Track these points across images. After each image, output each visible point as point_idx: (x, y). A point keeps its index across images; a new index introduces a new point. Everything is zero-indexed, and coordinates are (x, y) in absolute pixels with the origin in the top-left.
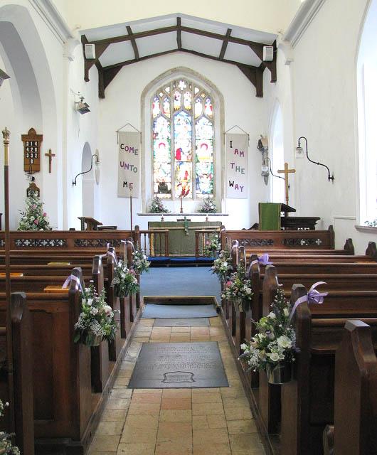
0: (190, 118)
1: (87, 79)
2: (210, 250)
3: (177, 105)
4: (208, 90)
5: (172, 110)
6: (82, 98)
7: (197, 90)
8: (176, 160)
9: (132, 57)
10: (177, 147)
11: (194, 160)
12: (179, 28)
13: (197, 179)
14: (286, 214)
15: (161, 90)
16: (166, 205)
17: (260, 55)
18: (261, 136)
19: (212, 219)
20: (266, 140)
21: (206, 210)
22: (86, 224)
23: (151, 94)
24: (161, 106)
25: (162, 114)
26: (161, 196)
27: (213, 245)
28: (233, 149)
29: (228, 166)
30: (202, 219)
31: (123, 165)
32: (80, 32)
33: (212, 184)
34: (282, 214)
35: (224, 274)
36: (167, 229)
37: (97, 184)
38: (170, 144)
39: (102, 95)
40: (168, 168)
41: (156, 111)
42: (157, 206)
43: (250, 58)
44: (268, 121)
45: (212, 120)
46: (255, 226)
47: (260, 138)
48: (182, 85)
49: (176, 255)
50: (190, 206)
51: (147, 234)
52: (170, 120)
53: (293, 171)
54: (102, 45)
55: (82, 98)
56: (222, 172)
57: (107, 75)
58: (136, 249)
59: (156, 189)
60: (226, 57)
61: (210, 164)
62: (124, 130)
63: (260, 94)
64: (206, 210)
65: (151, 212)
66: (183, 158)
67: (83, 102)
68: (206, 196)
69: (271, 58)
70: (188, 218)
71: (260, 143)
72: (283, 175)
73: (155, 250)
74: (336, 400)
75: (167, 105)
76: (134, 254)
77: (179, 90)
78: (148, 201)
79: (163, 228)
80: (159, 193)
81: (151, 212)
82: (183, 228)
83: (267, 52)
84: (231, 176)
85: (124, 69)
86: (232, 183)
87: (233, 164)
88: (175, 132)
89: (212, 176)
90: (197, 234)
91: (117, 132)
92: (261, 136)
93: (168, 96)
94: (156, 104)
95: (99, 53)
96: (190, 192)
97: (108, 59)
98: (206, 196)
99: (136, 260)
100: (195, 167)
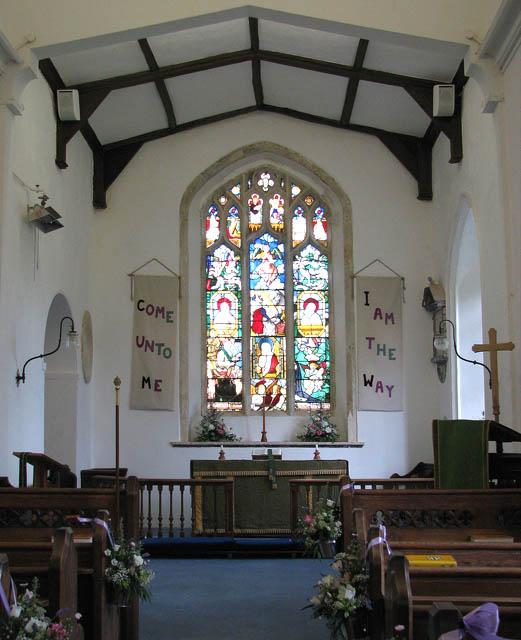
0: (281, 247)
1: (61, 163)
2: (315, 536)
3: (256, 220)
4: (319, 190)
5: (245, 230)
6: (45, 199)
7: (296, 191)
8: (253, 334)
9: (163, 124)
10: (254, 306)
11: (289, 330)
12: (255, 54)
13: (298, 372)
14: (499, 448)
15: (224, 191)
16: (232, 426)
17: (426, 104)
18: (430, 279)
19: (328, 454)
20: (441, 287)
21: (314, 436)
22: (30, 468)
23: (202, 199)
24: (223, 225)
25: (224, 240)
26: (221, 406)
27: (322, 524)
28: (371, 310)
29: (361, 344)
30: (305, 454)
31: (142, 343)
32: (34, 50)
33: (327, 381)
34: (492, 447)
35: (345, 621)
36: (230, 475)
37: (87, 380)
38: (241, 301)
39: (99, 202)
40: (235, 349)
41: (213, 234)
42: (212, 427)
43: (410, 119)
44: (444, 249)
45: (325, 249)
46: (420, 469)
47: (427, 284)
48: (265, 181)
49: (253, 531)
50: (280, 429)
51: (187, 488)
52: (243, 255)
53: (510, 347)
54: (93, 93)
55: (45, 199)
56: (349, 357)
57: (111, 161)
58: (117, 541)
59: (211, 390)
60: (355, 119)
61: (323, 340)
62: (144, 272)
63: (425, 194)
64: (314, 436)
65: (200, 439)
66: (269, 329)
67: (46, 206)
68: (315, 406)
69: (451, 109)
70: (277, 451)
71: (428, 293)
72: (480, 357)
73: (204, 520)
74: (192, 179)
75: (234, 223)
76: (108, 552)
77: (259, 190)
78: (196, 414)
79: (221, 473)
80: (216, 400)
81: (200, 439)
82: (264, 473)
83: (442, 98)
84: (369, 364)
85: (147, 149)
86: (368, 378)
87: (370, 339)
88: (252, 277)
89: (328, 364)
90: (296, 487)
91: (131, 275)
92: (430, 279)
93: (234, 202)
94: (213, 221)
95: (87, 106)
96: (282, 399)
97: (114, 120)
98: (315, 406)
99: (116, 569)
100: (291, 347)
